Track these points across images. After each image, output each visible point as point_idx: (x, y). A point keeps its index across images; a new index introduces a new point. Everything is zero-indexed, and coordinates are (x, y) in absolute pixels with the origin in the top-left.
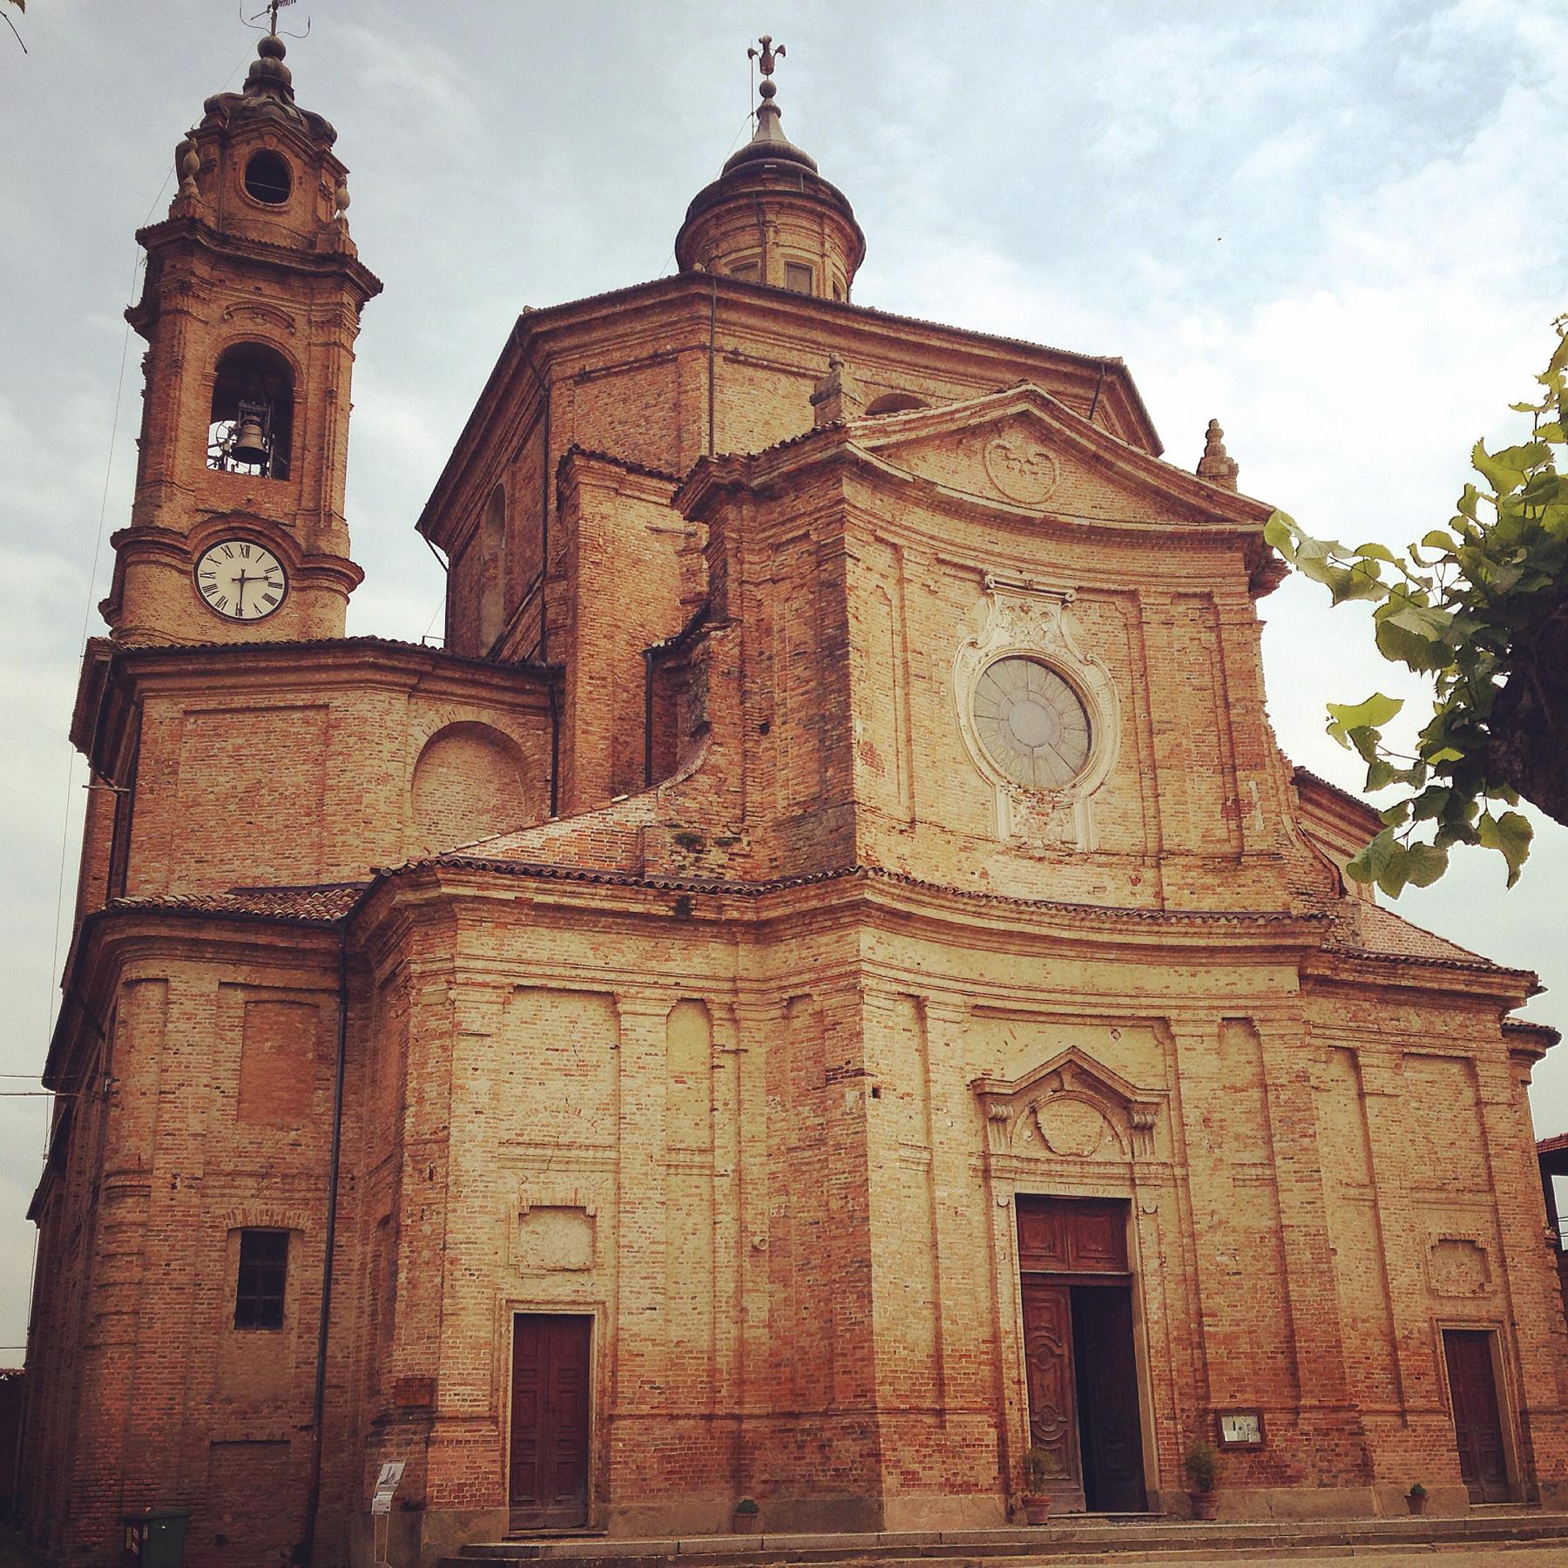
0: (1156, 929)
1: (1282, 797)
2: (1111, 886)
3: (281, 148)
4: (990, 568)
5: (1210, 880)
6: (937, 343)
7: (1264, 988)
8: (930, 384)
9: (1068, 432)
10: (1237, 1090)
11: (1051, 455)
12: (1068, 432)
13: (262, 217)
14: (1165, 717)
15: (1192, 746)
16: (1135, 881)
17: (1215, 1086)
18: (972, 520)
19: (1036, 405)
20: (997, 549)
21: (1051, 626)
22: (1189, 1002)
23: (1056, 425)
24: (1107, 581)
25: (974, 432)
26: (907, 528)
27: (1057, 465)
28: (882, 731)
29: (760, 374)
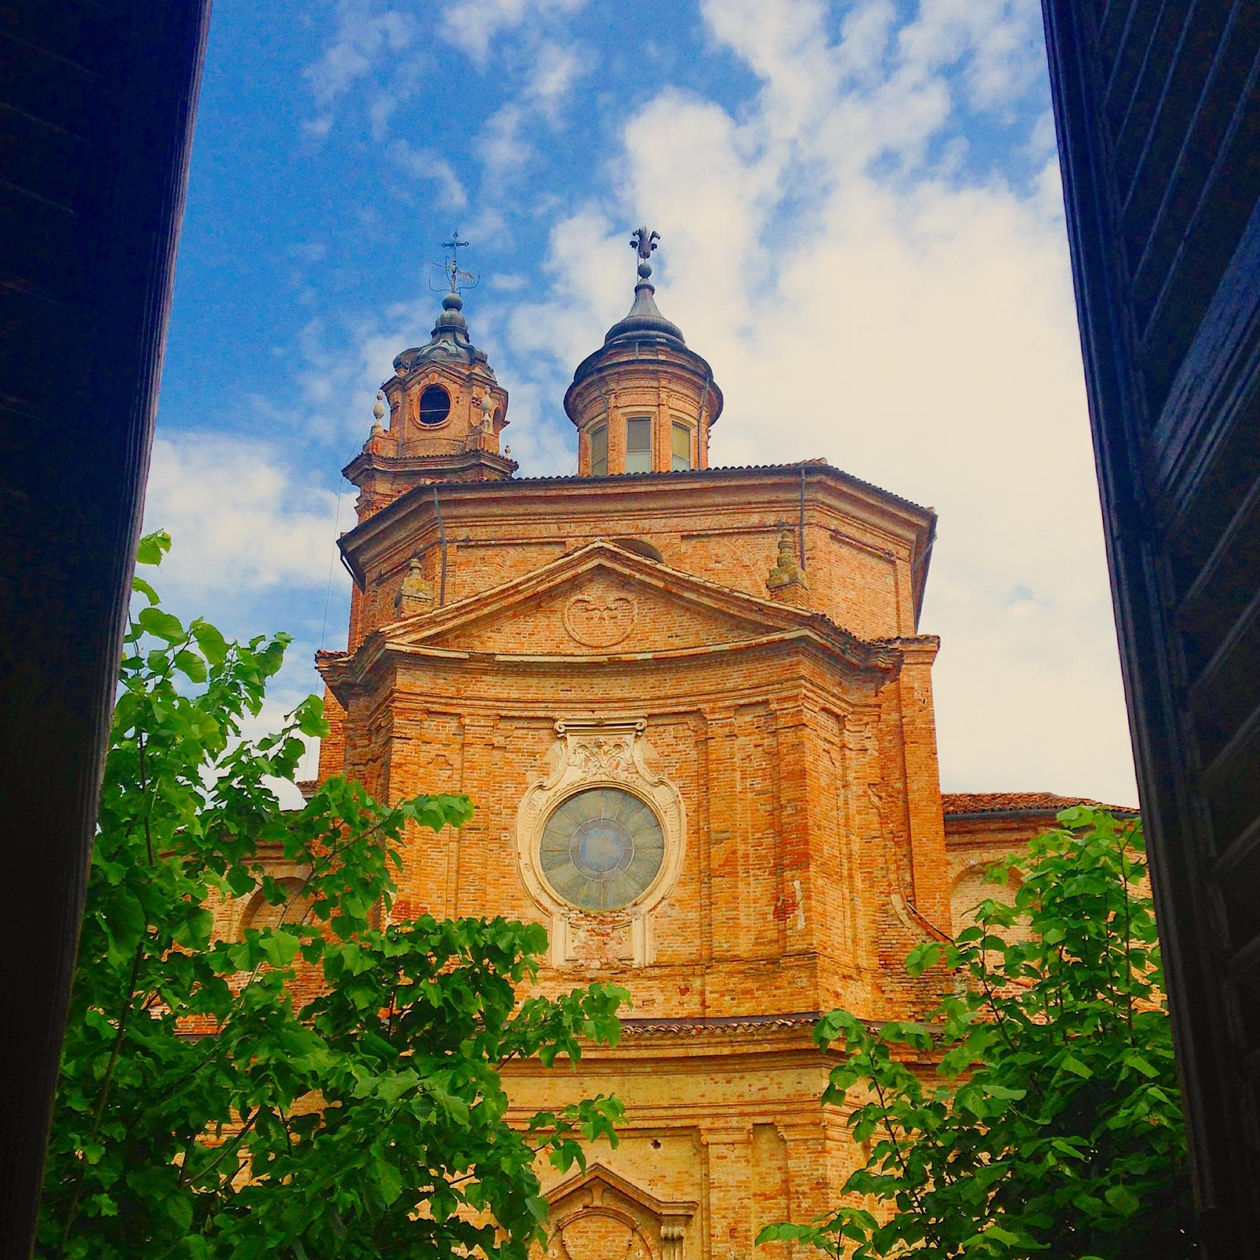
0: (681, 1042)
1: (892, 877)
2: (660, 998)
3: (442, 379)
4: (556, 715)
5: (750, 985)
6: (642, 489)
7: (792, 1092)
8: (646, 524)
9: (638, 576)
10: (767, 1198)
11: (630, 597)
12: (638, 576)
13: (429, 435)
14: (723, 826)
15: (751, 851)
16: (684, 991)
17: (743, 1195)
18: (545, 674)
19: (607, 558)
20: (570, 695)
21: (626, 755)
22: (721, 1111)
23: (627, 571)
24: (677, 705)
25: (551, 594)
26: (467, 698)
27: (636, 606)
28: (430, 885)
29: (490, 552)
